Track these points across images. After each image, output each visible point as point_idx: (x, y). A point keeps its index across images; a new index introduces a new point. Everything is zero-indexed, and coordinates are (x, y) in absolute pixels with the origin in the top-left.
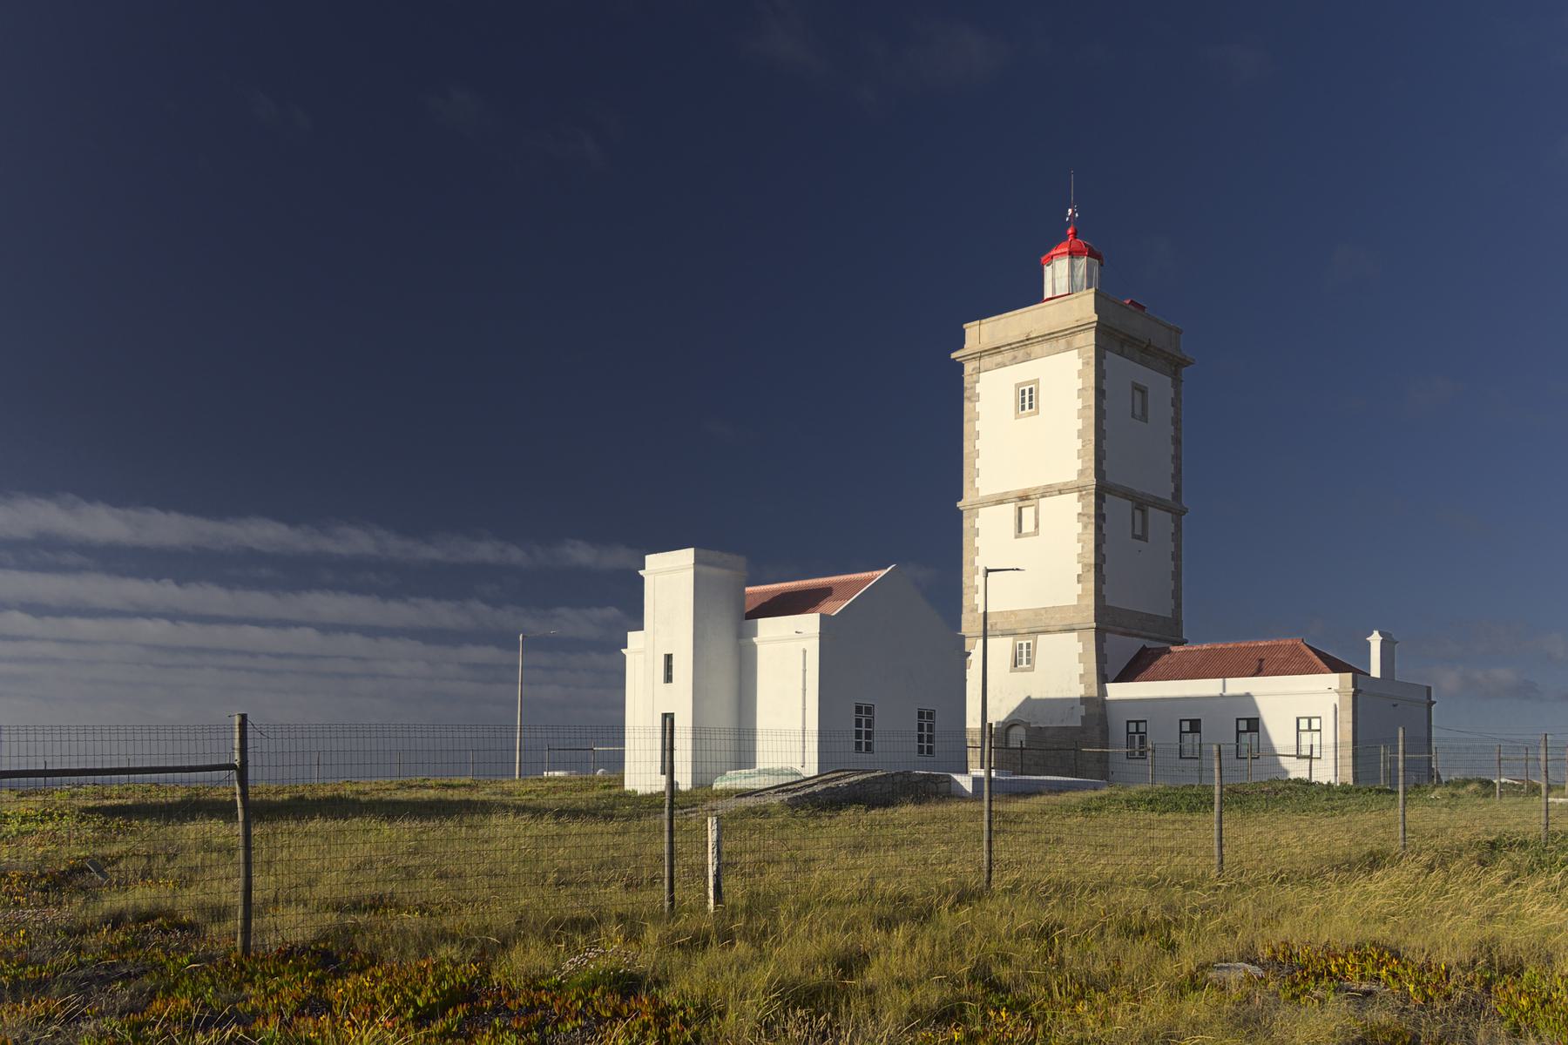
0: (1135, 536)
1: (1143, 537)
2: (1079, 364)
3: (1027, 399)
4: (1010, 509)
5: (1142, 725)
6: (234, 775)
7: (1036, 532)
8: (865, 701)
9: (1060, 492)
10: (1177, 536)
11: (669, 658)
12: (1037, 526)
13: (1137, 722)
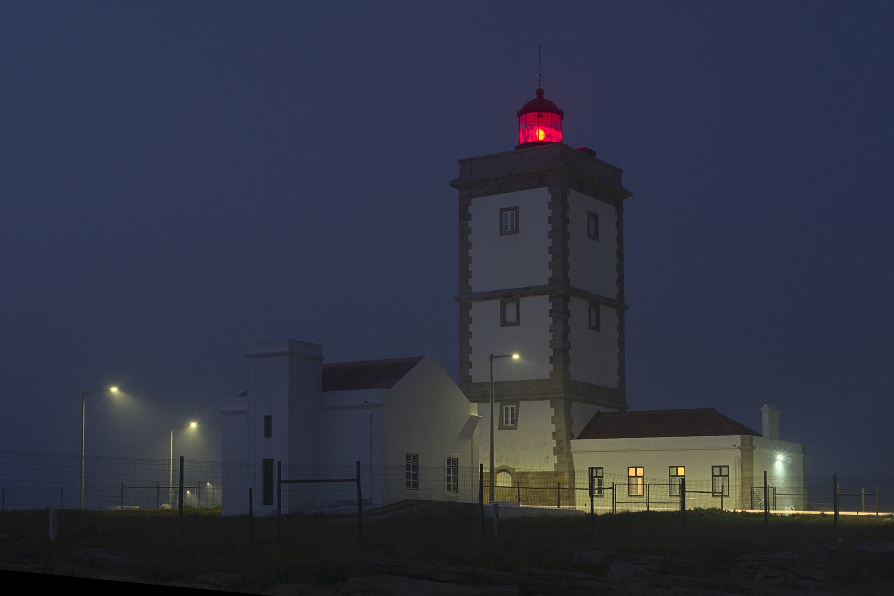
0: (591, 328)
1: (597, 328)
2: (548, 198)
3: (509, 223)
4: (497, 303)
5: (600, 471)
6: (355, 483)
7: (517, 323)
9: (536, 294)
10: (621, 327)
11: (268, 419)
12: (518, 318)
13: (720, 467)
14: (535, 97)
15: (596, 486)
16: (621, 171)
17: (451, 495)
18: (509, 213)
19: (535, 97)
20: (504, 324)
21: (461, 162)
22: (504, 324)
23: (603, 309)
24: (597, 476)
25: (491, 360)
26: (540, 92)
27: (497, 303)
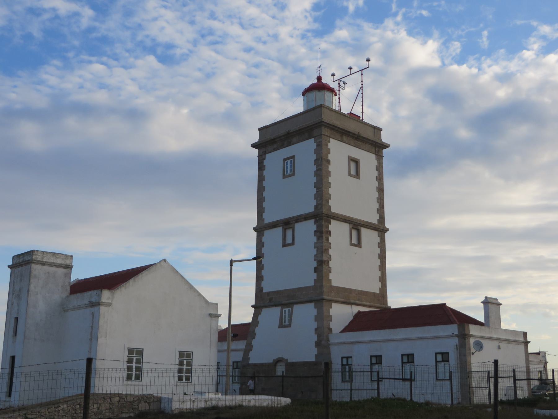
0: (351, 244)
4: (280, 230)
5: (350, 360)
8: (136, 345)
14: (316, 81)
15: (347, 374)
16: (381, 130)
17: (134, 389)
18: (289, 161)
19: (316, 81)
20: (285, 245)
21: (259, 129)
22: (285, 245)
23: (364, 231)
24: (347, 364)
25: (231, 265)
26: (319, 78)
27: (280, 230)
